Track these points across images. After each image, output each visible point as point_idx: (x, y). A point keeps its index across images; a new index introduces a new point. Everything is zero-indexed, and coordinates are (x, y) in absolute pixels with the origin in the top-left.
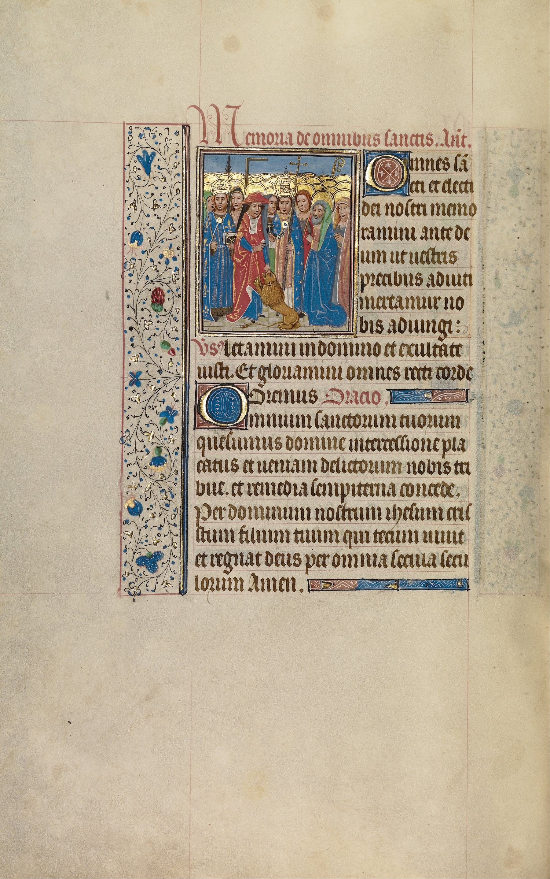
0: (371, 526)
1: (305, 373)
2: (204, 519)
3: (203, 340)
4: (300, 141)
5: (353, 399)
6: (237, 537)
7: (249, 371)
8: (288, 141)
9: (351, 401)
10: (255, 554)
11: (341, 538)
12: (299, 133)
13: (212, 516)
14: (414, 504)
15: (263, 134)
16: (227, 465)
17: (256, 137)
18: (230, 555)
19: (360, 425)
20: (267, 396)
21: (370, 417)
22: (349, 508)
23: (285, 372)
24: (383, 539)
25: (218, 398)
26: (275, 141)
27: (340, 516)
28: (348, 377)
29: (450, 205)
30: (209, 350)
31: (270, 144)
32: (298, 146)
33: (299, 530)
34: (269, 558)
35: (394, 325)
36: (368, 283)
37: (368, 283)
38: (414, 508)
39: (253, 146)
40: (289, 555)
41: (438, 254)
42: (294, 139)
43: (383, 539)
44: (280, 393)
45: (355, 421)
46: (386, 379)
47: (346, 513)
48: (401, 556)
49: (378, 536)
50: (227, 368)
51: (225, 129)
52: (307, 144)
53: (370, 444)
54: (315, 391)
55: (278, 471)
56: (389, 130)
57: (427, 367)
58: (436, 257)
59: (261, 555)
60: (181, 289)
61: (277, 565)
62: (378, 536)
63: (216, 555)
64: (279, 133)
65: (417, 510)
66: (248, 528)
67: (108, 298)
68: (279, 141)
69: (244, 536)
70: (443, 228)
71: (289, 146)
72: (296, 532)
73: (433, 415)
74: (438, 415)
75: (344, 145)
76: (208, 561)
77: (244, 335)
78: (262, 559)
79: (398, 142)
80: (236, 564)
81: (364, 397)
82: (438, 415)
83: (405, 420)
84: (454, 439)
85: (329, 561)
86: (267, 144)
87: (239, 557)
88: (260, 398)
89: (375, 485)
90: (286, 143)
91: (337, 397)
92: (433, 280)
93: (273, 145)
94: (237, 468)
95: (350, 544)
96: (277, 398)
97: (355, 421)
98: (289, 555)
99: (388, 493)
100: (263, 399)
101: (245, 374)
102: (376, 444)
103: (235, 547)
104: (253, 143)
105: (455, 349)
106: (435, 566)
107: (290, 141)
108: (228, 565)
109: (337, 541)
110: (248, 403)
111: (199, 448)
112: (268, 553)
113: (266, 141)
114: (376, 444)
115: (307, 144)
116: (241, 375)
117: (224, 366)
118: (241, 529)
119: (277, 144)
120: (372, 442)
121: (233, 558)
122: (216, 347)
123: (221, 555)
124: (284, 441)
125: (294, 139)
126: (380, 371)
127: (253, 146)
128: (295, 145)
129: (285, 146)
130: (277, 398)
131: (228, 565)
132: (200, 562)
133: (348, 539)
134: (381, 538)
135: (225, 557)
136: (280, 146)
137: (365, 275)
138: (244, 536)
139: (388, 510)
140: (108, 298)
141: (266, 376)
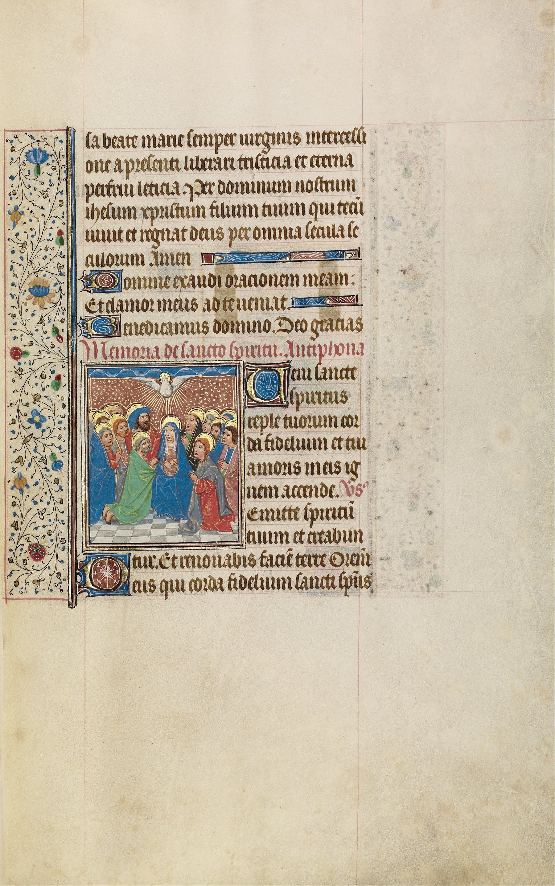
1: (259, 470)
2: (198, 193)
6: (208, 212)
7: (171, 560)
10: (180, 229)
14: (111, 204)
19: (113, 263)
21: (122, 256)
27: (318, 188)
29: (283, 276)
30: (355, 491)
34: (194, 232)
37: (157, 215)
39: (192, 359)
41: (326, 182)
45: (196, 585)
46: (233, 567)
47: (324, 185)
53: (326, 136)
56: (192, 130)
57: (154, 183)
58: (324, 185)
59: (186, 230)
60: (67, 375)
61: (201, 239)
65: (113, 209)
72: (264, 206)
73: (146, 347)
78: (187, 235)
80: (163, 239)
84: (334, 226)
85: (250, 234)
87: (166, 233)
88: (289, 327)
89: (249, 159)
90: (153, 357)
97: (196, 585)
99: (337, 235)
101: (168, 563)
102: (333, 161)
105: (130, 141)
108: (156, 241)
114: (333, 161)
115: (176, 357)
117: (180, 206)
120: (328, 134)
121: (160, 234)
122: (362, 488)
125: (161, 353)
127: (192, 359)
133: (313, 211)
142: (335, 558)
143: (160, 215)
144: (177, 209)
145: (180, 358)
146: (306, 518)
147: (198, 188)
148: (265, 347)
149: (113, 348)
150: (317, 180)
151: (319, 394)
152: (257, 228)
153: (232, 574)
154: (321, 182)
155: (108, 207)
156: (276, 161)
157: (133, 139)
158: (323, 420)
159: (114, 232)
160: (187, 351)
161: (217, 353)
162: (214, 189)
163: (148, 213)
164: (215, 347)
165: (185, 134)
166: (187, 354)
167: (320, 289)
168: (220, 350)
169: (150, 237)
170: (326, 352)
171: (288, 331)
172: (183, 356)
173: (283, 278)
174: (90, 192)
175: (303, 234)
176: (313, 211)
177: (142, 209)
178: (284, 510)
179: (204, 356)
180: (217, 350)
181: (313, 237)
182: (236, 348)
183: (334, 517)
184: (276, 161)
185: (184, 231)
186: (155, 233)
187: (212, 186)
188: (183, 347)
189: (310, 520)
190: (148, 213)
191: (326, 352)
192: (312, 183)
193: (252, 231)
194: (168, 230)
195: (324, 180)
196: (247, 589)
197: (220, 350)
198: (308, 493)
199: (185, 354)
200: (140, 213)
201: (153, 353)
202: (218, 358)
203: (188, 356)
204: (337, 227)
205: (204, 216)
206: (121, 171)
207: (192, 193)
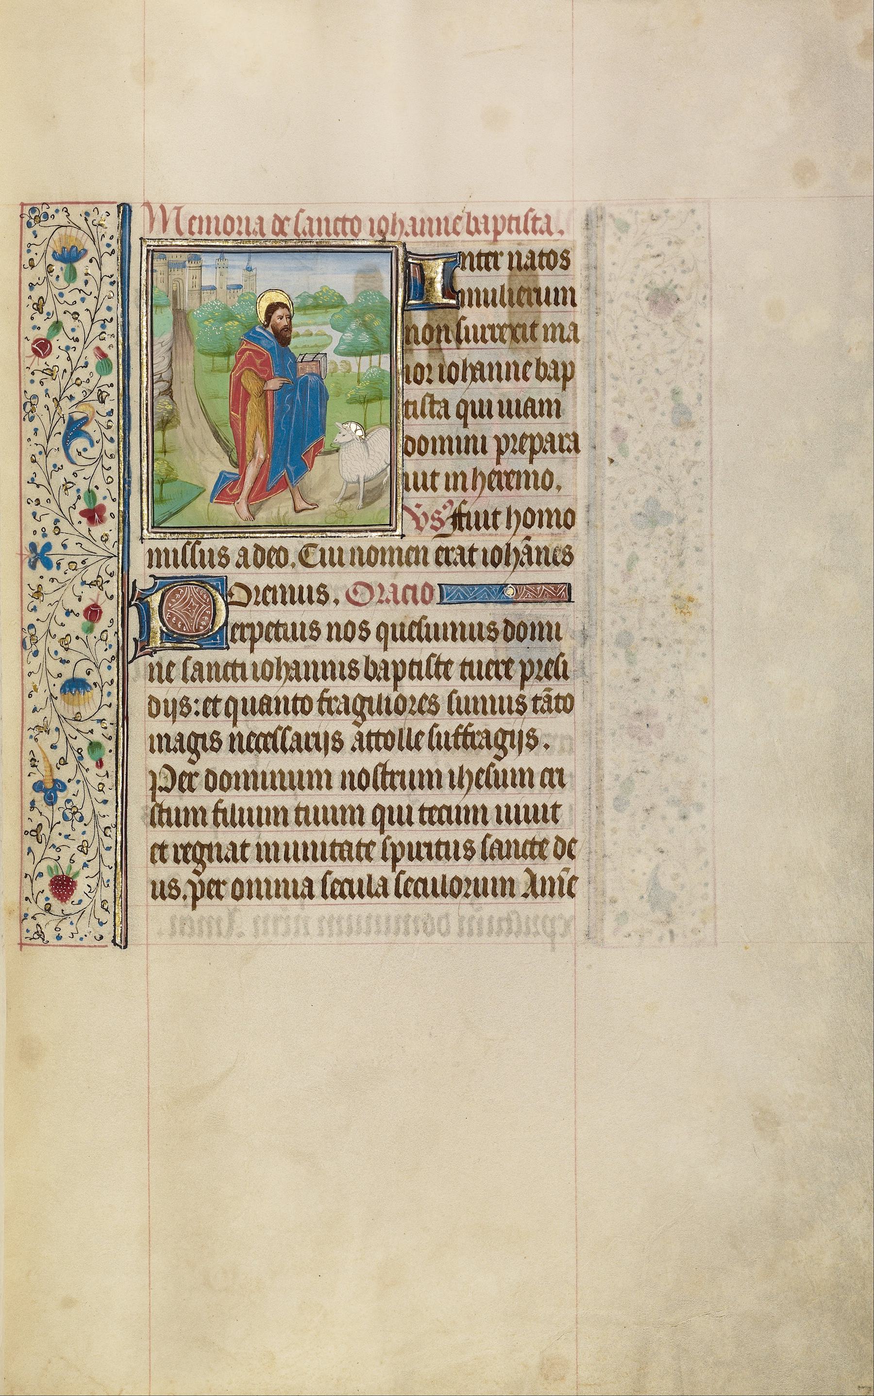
5: (391, 597)
8: (257, 229)
9: (388, 601)
13: (177, 786)
16: (162, 889)
18: (202, 847)
20: (254, 594)
24: (435, 818)
25: (182, 591)
26: (236, 229)
31: (228, 234)
33: (303, 805)
35: (361, 741)
36: (532, 673)
37: (532, 673)
38: (424, 622)
40: (457, 844)
41: (392, 774)
43: (435, 818)
44: (274, 589)
51: (171, 226)
54: (325, 587)
56: (302, 211)
58: (388, 778)
63: (181, 845)
66: (226, 804)
68: (243, 229)
69: (220, 816)
70: (359, 842)
71: (259, 237)
72: (298, 810)
74: (505, 696)
75: (328, 234)
76: (170, 853)
79: (315, 229)
80: (210, 859)
81: (410, 593)
82: (505, 696)
83: (302, 814)
86: (222, 233)
92: (361, 741)
93: (234, 236)
94: (228, 562)
95: (382, 826)
96: (269, 598)
98: (457, 844)
100: (249, 600)
103: (205, 835)
104: (200, 232)
107: (261, 229)
110: (227, 605)
112: (558, 839)
113: (221, 229)
116: (357, 599)
117: (165, 807)
118: (217, 805)
123: (189, 845)
125: (267, 229)
126: (472, 442)
129: (252, 237)
130: (269, 598)
131: (502, 747)
132: (210, 710)
133: (462, 413)
134: (431, 817)
135: (416, 884)
136: (244, 236)
138: (220, 816)
139: (452, 773)
141: (507, 744)
142: (355, 592)
144: (438, 664)
146: (384, 858)
148: (439, 844)
149: (194, 218)
151: (428, 845)
152: (237, 881)
153: (221, 801)
154: (384, 773)
157: (367, 846)
160: (303, 224)
161: (348, 229)
164: (344, 220)
166: (541, 228)
167: (510, 312)
169: (190, 857)
170: (403, 854)
172: (296, 232)
173: (491, 666)
175: (317, 889)
176: (462, 413)
178: (296, 699)
180: (348, 224)
182: (393, 845)
185: (244, 846)
186: (198, 849)
188: (297, 217)
191: (403, 854)
193: (230, 885)
194: (219, 846)
195: (389, 769)
196: (265, 566)
198: (513, 483)
199: (251, 230)
201: (254, 226)
203: (254, 232)
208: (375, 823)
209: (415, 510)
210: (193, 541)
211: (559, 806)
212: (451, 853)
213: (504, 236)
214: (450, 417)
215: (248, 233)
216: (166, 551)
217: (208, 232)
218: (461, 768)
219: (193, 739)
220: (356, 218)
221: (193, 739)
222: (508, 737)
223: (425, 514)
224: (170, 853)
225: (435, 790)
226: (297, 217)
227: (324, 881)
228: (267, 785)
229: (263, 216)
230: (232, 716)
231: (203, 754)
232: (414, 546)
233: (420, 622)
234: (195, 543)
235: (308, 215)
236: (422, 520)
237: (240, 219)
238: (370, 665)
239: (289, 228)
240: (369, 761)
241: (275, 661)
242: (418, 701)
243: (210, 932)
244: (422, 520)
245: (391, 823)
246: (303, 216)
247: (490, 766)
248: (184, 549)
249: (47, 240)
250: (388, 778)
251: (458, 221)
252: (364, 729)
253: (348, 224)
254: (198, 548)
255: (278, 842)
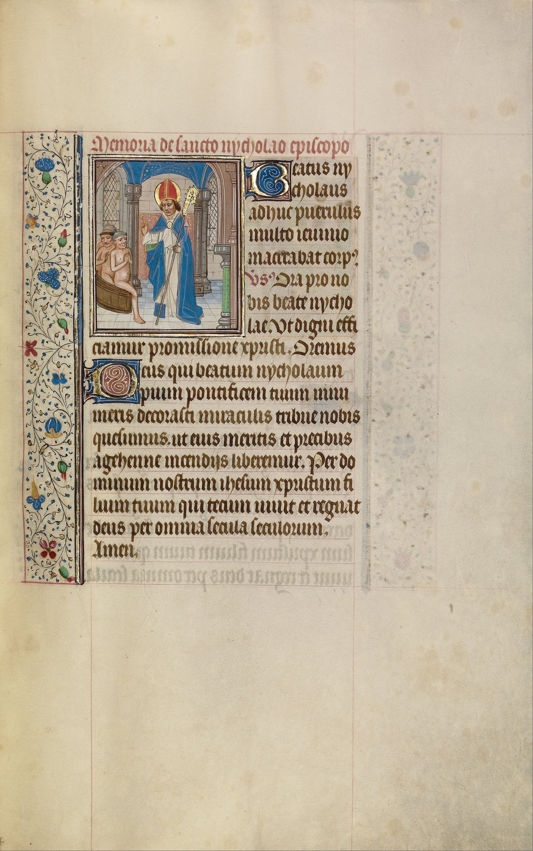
0: (205, 496)
2: (318, 466)
3: (253, 271)
4: (164, 147)
8: (151, 148)
11: (177, 508)
12: (163, 140)
15: (127, 141)
17: (120, 144)
22: (248, 434)
23: (318, 280)
24: (217, 508)
26: (337, 261)
28: (198, 375)
30: (260, 281)
31: (134, 150)
32: (162, 153)
35: (254, 213)
38: (246, 478)
41: (186, 480)
42: (158, 147)
43: (217, 508)
48: (321, 142)
49: (212, 505)
50: (282, 345)
52: (171, 151)
55: (329, 489)
56: (181, 136)
58: (184, 483)
61: (253, 466)
62: (212, 505)
64: (143, 141)
67: (451, 606)
68: (142, 147)
75: (197, 151)
76: (310, 507)
77: (104, 335)
80: (337, 511)
83: (274, 394)
90: (149, 150)
91: (283, 280)
92: (254, 213)
94: (328, 171)
105: (300, 302)
106: (246, 533)
109: (215, 489)
111: (95, 443)
115: (171, 151)
119: (140, 150)
124: (271, 301)
125: (158, 147)
128: (159, 152)
129: (181, 153)
132: (303, 509)
133: (172, 373)
137: (233, 398)
139: (222, 481)
140: (451, 606)
141: (333, 511)
143: (165, 419)
144: (181, 480)
145: (175, 152)
147: (318, 460)
150: (176, 477)
155: (243, 478)
156: (241, 416)
158: (256, 483)
159: (179, 436)
160: (182, 146)
161: (209, 148)
162: (336, 463)
163: (248, 348)
164: (207, 142)
165: (175, 138)
168: (212, 145)
171: (285, 286)
172: (178, 150)
174: (136, 531)
177: (275, 480)
179: (117, 149)
180: (210, 145)
181: (215, 533)
183: (254, 444)
184: (241, 416)
186: (329, 505)
187: (335, 460)
188: (178, 141)
189: (249, 354)
190: (248, 348)
192: (171, 481)
195: (184, 478)
197: (212, 145)
199: (180, 149)
200: (273, 485)
202: (211, 153)
204: (239, 523)
205: (148, 489)
206: (301, 285)
207: (312, 466)
208: (180, 511)
209: (251, 274)
210: (204, 339)
211: (360, 503)
212: (111, 530)
213: (304, 154)
214: (320, 263)
215: (145, 150)
216: (124, 344)
217: (122, 150)
218: (228, 478)
219: (313, 324)
220: (215, 141)
221: (313, 324)
222: (317, 326)
223: (256, 276)
224: (310, 507)
225: (145, 491)
226: (178, 141)
227: (253, 523)
228: (224, 487)
229: (275, 140)
230: (97, 445)
231: (113, 469)
232: (98, 343)
233: (243, 478)
234: (205, 339)
235: (185, 139)
236: (255, 278)
237: (140, 142)
238: (296, 414)
239: (174, 147)
240: (172, 473)
241: (338, 412)
242: (308, 437)
243: (165, 579)
244: (255, 278)
245: (191, 511)
246: (182, 140)
247: (244, 476)
248: (198, 344)
249: (32, 155)
250: (184, 483)
251: (171, 143)
252: (102, 455)
253: (210, 145)
254: (206, 342)
255: (189, 522)
